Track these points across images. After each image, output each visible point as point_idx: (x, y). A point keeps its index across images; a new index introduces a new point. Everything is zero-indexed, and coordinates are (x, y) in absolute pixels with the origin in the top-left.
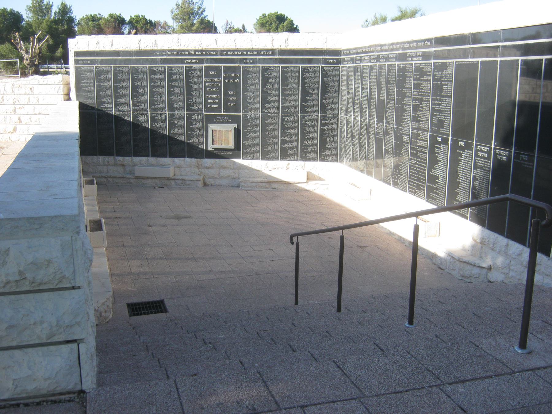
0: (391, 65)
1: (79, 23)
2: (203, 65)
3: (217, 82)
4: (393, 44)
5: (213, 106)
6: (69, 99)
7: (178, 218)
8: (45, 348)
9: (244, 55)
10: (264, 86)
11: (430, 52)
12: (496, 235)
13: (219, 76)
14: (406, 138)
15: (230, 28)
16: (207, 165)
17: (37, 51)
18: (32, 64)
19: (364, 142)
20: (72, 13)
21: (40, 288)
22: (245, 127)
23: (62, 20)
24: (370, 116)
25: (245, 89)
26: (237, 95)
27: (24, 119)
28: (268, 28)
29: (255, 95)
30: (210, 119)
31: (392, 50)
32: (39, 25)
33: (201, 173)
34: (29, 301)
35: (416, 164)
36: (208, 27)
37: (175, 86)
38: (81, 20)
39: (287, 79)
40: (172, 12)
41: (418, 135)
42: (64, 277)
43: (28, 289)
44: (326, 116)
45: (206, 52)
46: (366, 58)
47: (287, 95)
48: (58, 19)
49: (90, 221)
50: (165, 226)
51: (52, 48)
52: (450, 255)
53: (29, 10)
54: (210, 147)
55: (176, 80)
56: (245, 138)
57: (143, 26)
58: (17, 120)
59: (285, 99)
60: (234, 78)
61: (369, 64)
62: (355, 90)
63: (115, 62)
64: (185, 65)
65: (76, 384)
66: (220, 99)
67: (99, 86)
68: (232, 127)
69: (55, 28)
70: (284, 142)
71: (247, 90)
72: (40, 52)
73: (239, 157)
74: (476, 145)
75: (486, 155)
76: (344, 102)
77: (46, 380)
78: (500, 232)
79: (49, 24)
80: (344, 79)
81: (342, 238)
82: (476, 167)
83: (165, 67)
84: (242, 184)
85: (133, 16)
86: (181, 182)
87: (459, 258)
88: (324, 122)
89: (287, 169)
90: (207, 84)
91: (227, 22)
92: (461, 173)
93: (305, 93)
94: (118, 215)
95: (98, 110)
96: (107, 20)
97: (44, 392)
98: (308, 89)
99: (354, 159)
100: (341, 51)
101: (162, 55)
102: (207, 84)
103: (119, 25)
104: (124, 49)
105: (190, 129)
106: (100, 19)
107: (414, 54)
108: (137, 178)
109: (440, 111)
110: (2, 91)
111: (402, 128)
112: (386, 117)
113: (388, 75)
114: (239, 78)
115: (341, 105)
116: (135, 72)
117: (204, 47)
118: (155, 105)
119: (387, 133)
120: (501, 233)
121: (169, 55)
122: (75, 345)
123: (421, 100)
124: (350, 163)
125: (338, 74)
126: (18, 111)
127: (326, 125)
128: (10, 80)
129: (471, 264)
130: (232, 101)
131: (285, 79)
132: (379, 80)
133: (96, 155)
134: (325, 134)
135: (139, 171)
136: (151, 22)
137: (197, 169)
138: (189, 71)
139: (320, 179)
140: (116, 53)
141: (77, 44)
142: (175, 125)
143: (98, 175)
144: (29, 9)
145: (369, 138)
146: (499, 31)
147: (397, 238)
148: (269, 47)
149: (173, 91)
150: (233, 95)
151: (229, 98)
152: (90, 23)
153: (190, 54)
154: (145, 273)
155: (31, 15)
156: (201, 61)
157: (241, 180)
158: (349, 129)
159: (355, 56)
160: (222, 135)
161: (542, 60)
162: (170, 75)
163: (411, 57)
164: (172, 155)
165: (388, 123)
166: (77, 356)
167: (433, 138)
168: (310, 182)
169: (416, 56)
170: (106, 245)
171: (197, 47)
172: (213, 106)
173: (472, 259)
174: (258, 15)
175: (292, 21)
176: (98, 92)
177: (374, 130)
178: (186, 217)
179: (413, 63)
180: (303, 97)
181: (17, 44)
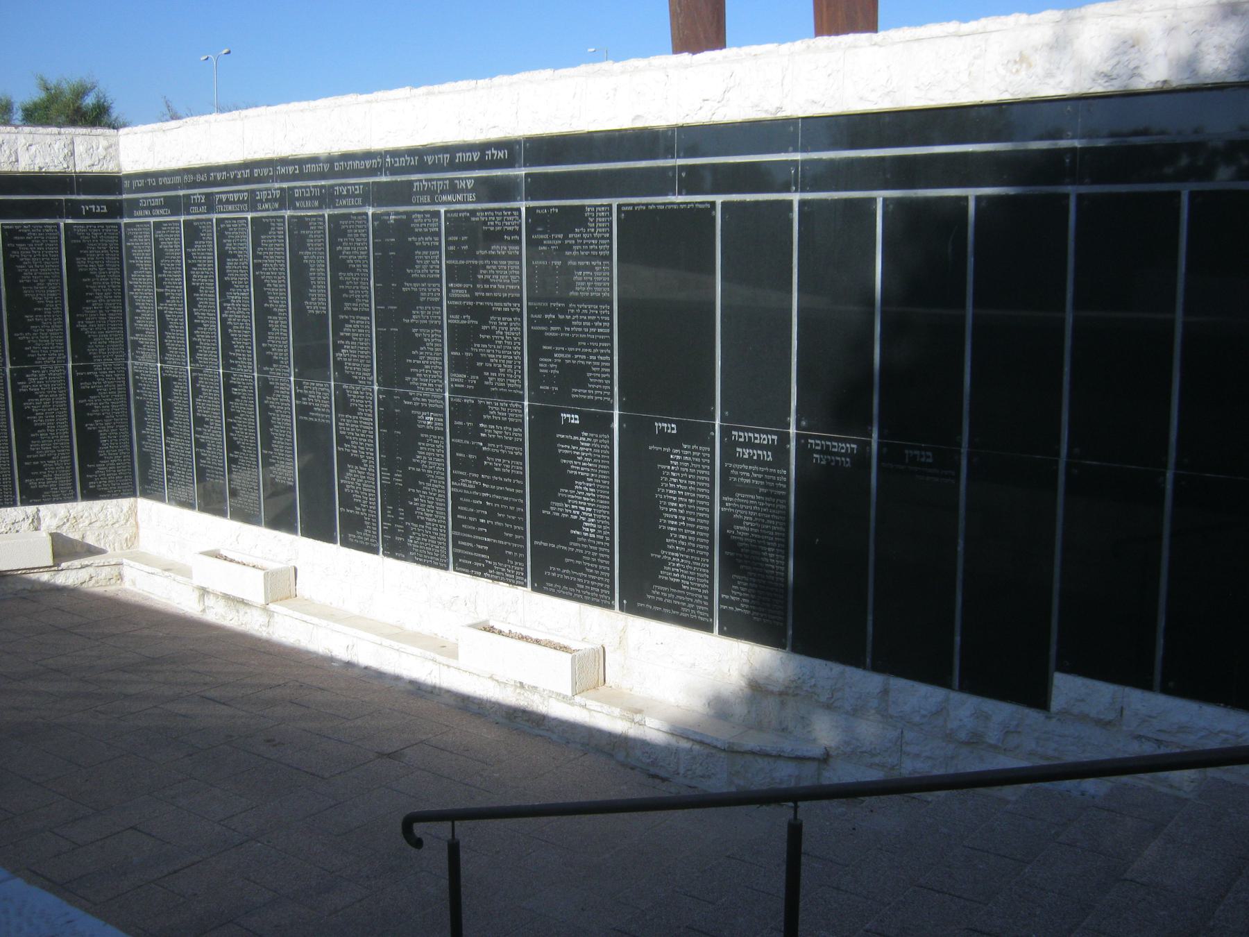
0: (346, 217)
12: (837, 668)
24: (266, 360)
35: (479, 488)
44: (91, 368)
52: (679, 732)
74: (725, 432)
83: (58, 225)
98: (27, 293)
100: (119, 178)
111: (411, 393)
115: (134, 332)
120: (852, 657)
127: (93, 392)
134: (91, 420)
139: (92, 551)
158: (175, 400)
161: (966, 198)
168: (64, 565)
169: (453, 188)
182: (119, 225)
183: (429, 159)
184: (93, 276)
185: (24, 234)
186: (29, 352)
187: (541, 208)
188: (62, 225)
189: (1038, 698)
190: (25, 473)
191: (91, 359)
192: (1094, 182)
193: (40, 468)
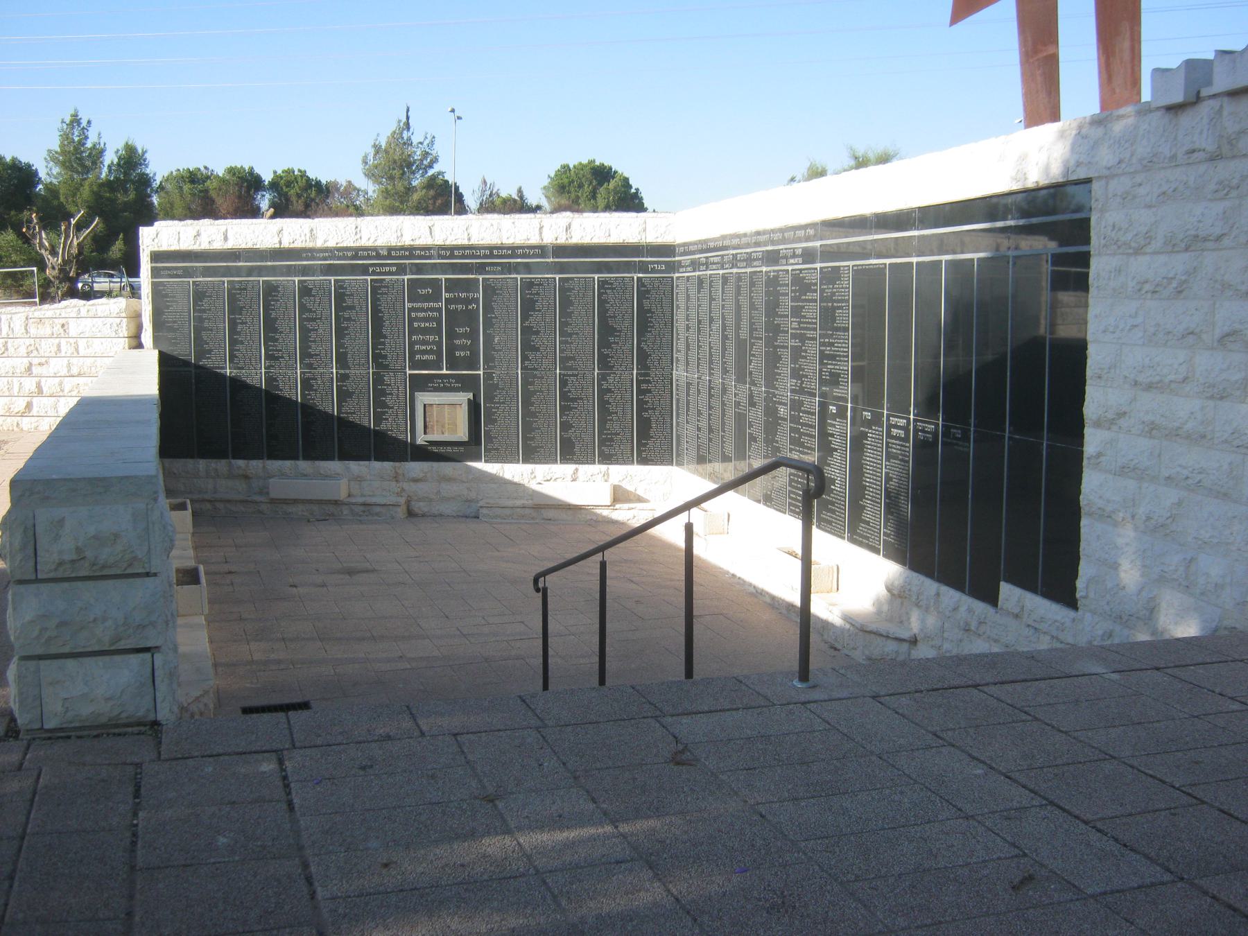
1: (161, 187)
2: (406, 278)
3: (432, 310)
4: (758, 233)
5: (426, 357)
6: (140, 346)
7: (351, 572)
8: (107, 658)
9: (485, 257)
10: (525, 317)
11: (814, 249)
12: (922, 578)
13: (436, 297)
14: (783, 411)
15: (491, 195)
16: (413, 475)
17: (75, 251)
18: (64, 276)
19: (717, 424)
20: (147, 166)
21: (104, 573)
22: (489, 398)
23: (126, 181)
24: (725, 371)
25: (488, 323)
26: (473, 335)
27: (49, 385)
28: (573, 195)
29: (510, 337)
30: (420, 384)
31: (757, 244)
32: (76, 190)
33: (403, 490)
34: (88, 592)
36: (443, 198)
37: (349, 319)
38: (167, 180)
39: (571, 303)
40: (365, 163)
41: (801, 403)
42: (135, 558)
43: (86, 574)
44: (648, 375)
45: (411, 251)
46: (716, 259)
47: (570, 335)
48: (117, 179)
49: (178, 571)
50: (324, 585)
51: (101, 242)
53: (54, 159)
54: (421, 439)
55: (352, 308)
56: (491, 420)
57: (301, 196)
58: (34, 388)
59: (566, 342)
60: (467, 301)
61: (721, 272)
62: (699, 322)
63: (228, 272)
64: (369, 278)
65: (148, 710)
66: (439, 344)
67: (200, 320)
68: (463, 398)
69: (108, 199)
70: (565, 426)
71: (492, 325)
72: (80, 253)
73: (477, 458)
75: (902, 433)
76: (682, 346)
77: (107, 700)
78: (929, 574)
79: (95, 189)
80: (681, 301)
81: (603, 565)
82: (889, 456)
84: (484, 511)
85: (279, 172)
86: (362, 508)
87: (862, 626)
88: (644, 386)
89: (574, 480)
90: (413, 315)
91: (485, 182)
92: (868, 470)
93: (607, 331)
94: (233, 568)
95: (197, 367)
96: (223, 181)
97: (103, 720)
99: (701, 460)
101: (325, 259)
102: (413, 315)
103: (248, 191)
104: (250, 246)
105: (379, 404)
106: (208, 177)
107: (790, 253)
108: (273, 501)
109: (833, 357)
110: (5, 330)
112: (751, 373)
113: (751, 292)
114: (476, 301)
115: (678, 351)
116: (271, 290)
117: (407, 241)
118: (311, 356)
119: (752, 404)
121: (339, 258)
122: (148, 656)
123: (803, 338)
124: (692, 467)
125: (668, 288)
126: (35, 370)
127: (650, 391)
128: (20, 309)
129: (881, 635)
130: (463, 348)
131: (566, 303)
132: (737, 301)
133: (192, 457)
134: (646, 410)
135: (278, 488)
136: (318, 183)
137: (394, 484)
138: (376, 287)
139: (640, 500)
140: (234, 255)
141: (157, 237)
142: (350, 395)
143: (195, 497)
144: (52, 157)
145: (724, 415)
146: (912, 211)
147: (768, 600)
148: (534, 240)
149: (347, 328)
150: (465, 336)
151: (457, 342)
152: (187, 187)
153: (379, 256)
154: (279, 662)
155: (56, 170)
156: (401, 270)
157: (481, 504)
159: (697, 256)
160: (444, 415)
162: (340, 297)
163: (786, 257)
164: (344, 456)
165: (753, 383)
166: (150, 670)
167: (824, 406)
168: (617, 506)
169: (794, 256)
170: (206, 611)
171: (393, 242)
172: (426, 357)
173: (884, 627)
174: (553, 168)
175: (626, 180)
176: (198, 331)
177: (731, 398)
178: (367, 571)
179: (790, 268)
180: (606, 338)
181: (34, 236)
189: (990, 597)
190: (602, 443)
191: (649, 368)
193: (612, 440)
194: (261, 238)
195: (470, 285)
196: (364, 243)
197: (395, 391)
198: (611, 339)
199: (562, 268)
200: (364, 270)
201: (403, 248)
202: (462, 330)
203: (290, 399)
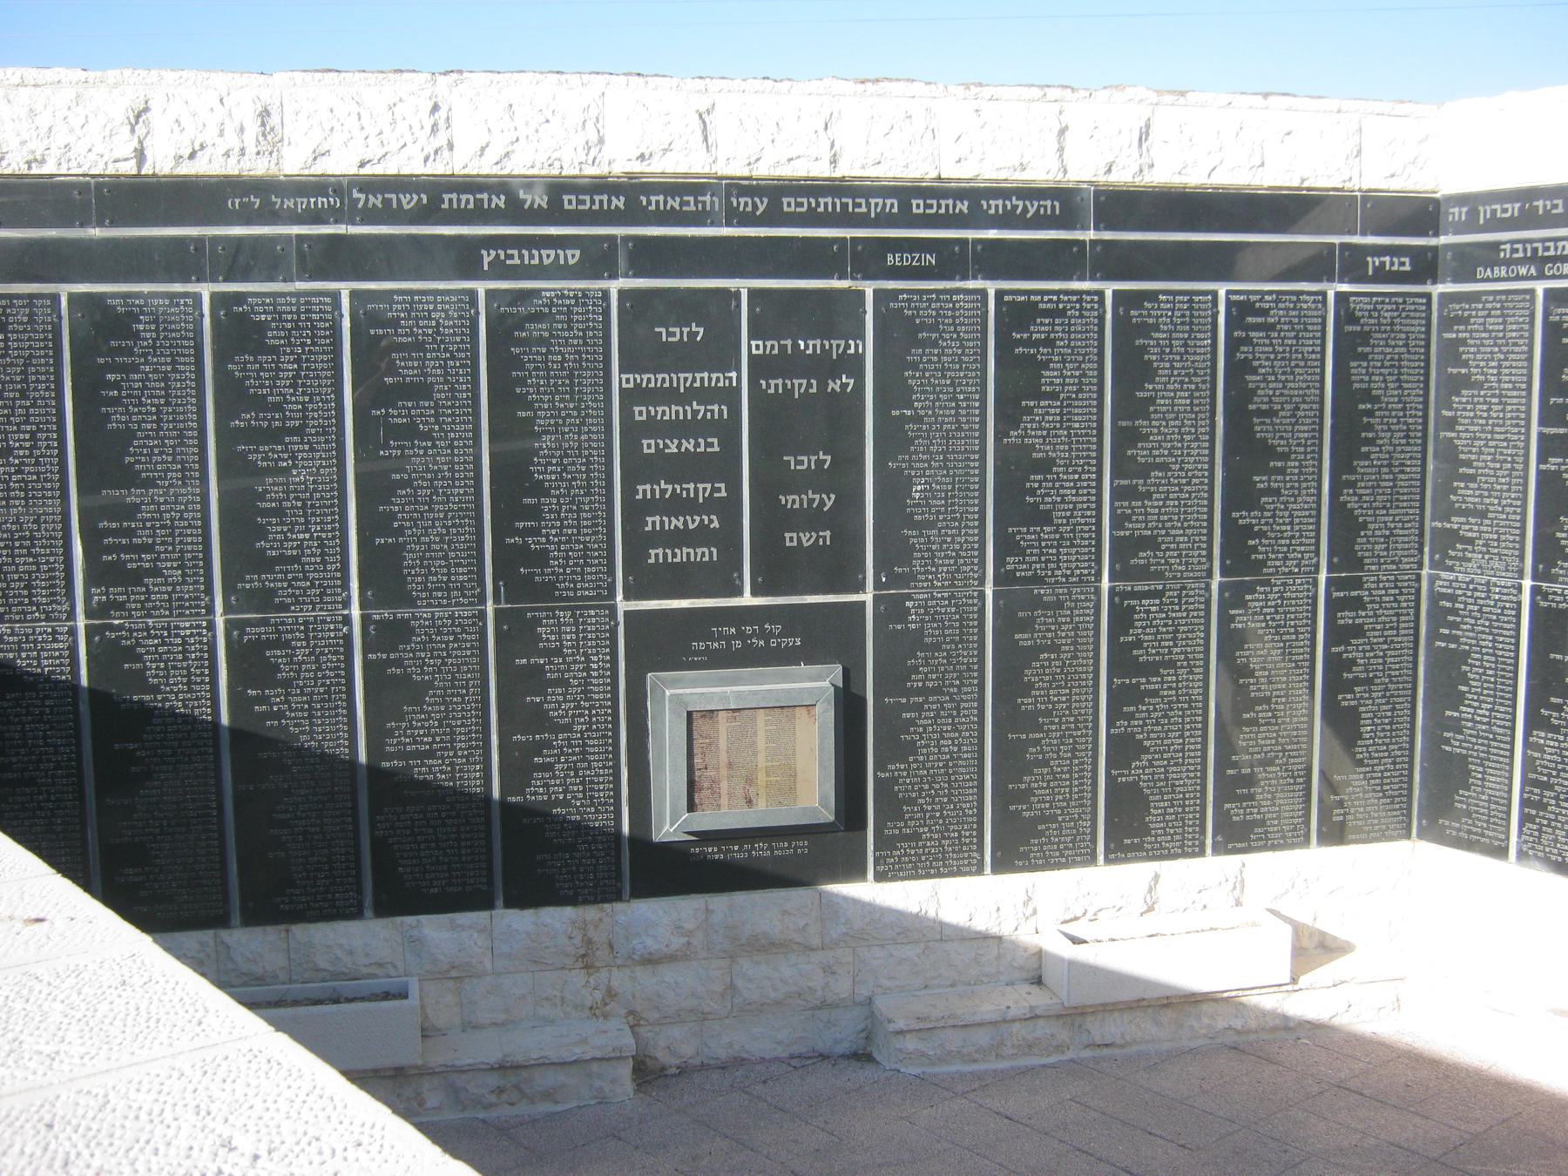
2: (614, 286)
5: (682, 555)
9: (884, 220)
10: (1009, 415)
13: (721, 353)
25: (892, 439)
30: (665, 645)
33: (611, 994)
37: (410, 432)
39: (1148, 372)
44: (1358, 584)
45: (633, 196)
54: (669, 826)
55: (421, 391)
56: (895, 747)
60: (825, 367)
64: (481, 287)
68: (816, 683)
70: (1124, 749)
71: (905, 444)
73: (854, 870)
86: (493, 1080)
88: (1346, 618)
90: (640, 413)
98: (1260, 429)
100: (1436, 202)
101: (316, 217)
102: (640, 413)
114: (854, 365)
116: (106, 328)
117: (618, 161)
121: (370, 217)
127: (1358, 631)
130: (812, 519)
134: (1349, 687)
137: (578, 977)
142: (416, 693)
148: (1041, 171)
151: (790, 501)
153: (516, 212)
156: (599, 259)
160: (748, 740)
162: (370, 354)
171: (573, 163)
172: (682, 555)
182: (1428, 296)
183: (569, 202)
184: (1376, 400)
185: (1264, 312)
186: (1254, 549)
187: (114, 295)
188: (1222, 294)
192: (1455, 281)
194: (61, 138)
195: (835, 314)
196: (463, 161)
197: (575, 675)
198: (1261, 481)
199: (1113, 262)
200: (465, 258)
201: (601, 186)
202: (806, 462)
203: (190, 721)
